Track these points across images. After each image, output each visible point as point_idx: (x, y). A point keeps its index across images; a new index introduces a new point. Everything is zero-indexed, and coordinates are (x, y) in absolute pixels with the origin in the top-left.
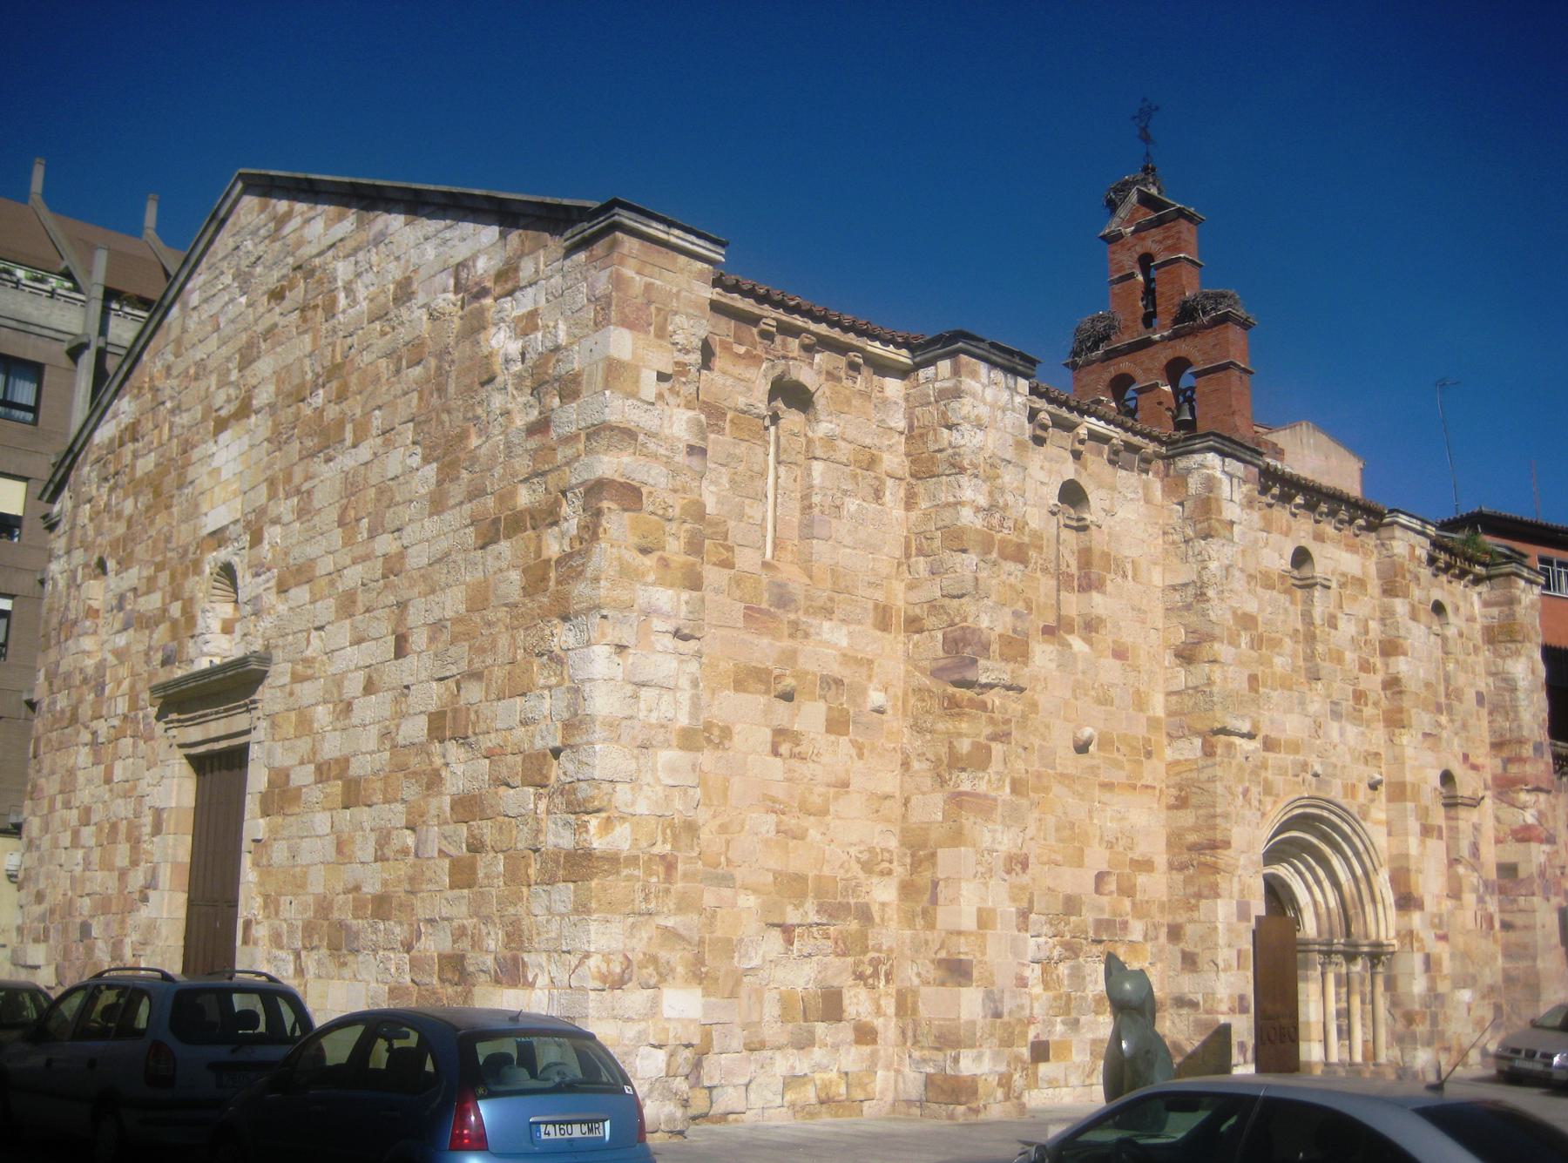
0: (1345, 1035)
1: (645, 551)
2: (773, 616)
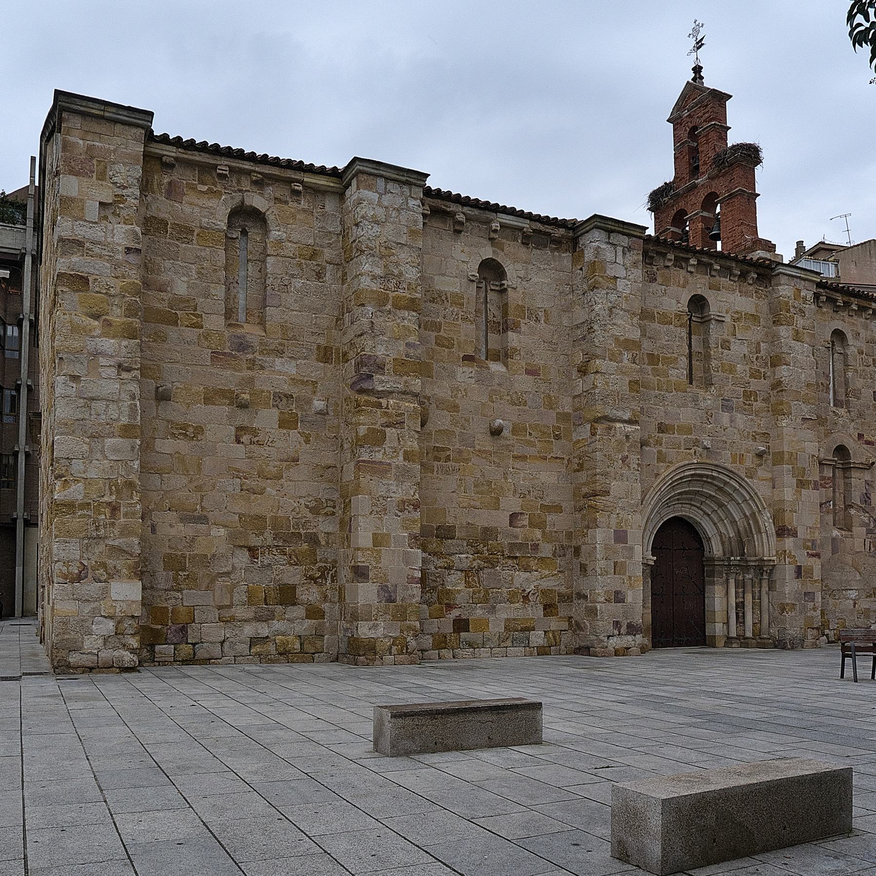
1: (96, 317)
2: (235, 357)
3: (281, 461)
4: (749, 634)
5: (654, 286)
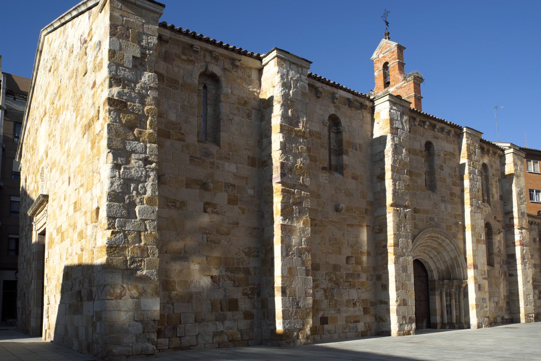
0: (449, 313)
3: (229, 224)
4: (454, 321)
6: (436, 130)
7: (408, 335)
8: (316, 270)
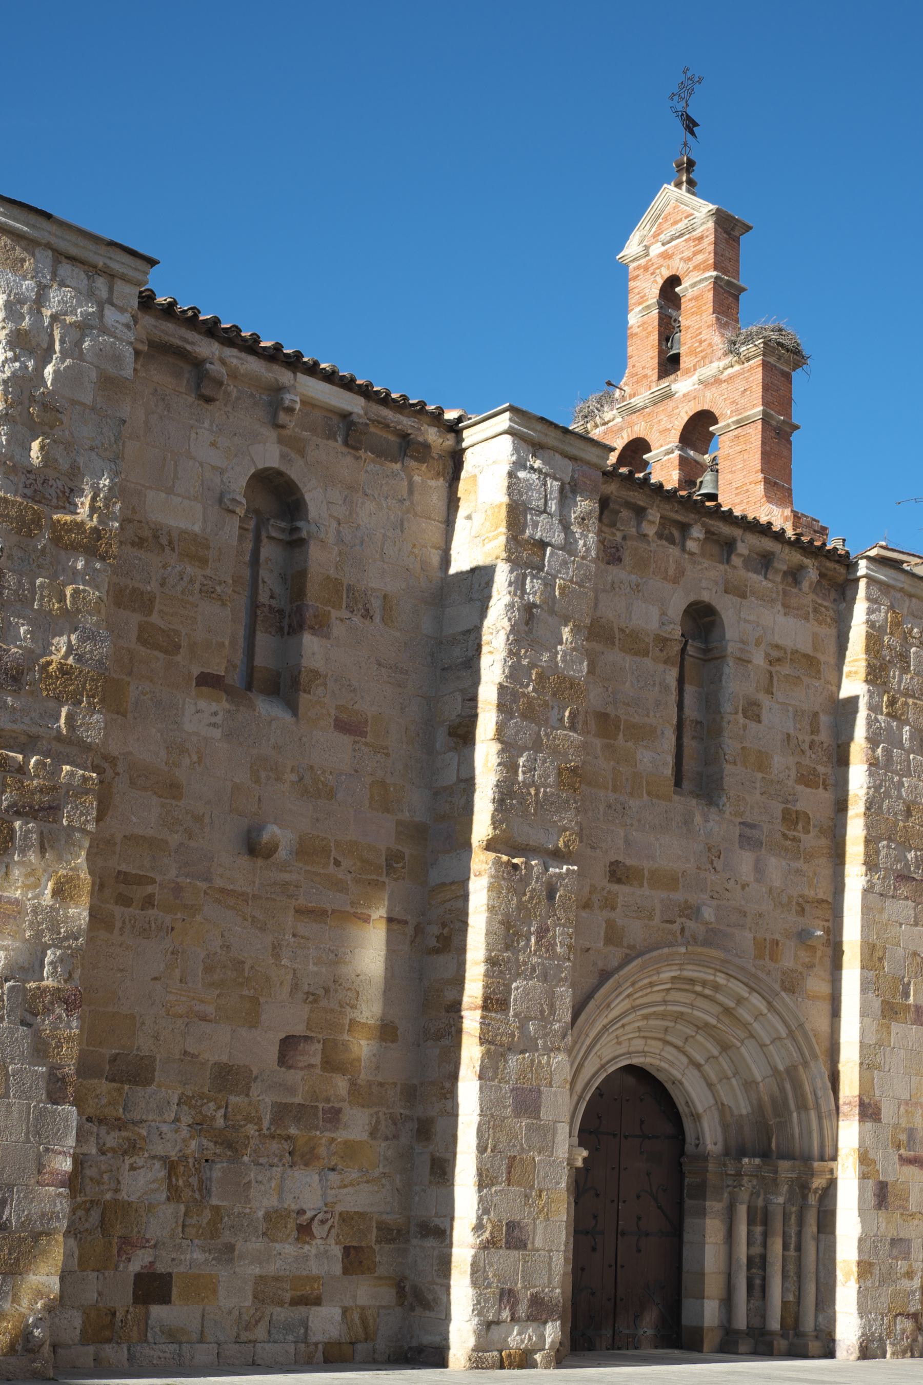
0: (757, 1292)
4: (775, 1324)
5: (616, 573)
6: (736, 561)
7: (521, 1367)
8: (136, 1083)
